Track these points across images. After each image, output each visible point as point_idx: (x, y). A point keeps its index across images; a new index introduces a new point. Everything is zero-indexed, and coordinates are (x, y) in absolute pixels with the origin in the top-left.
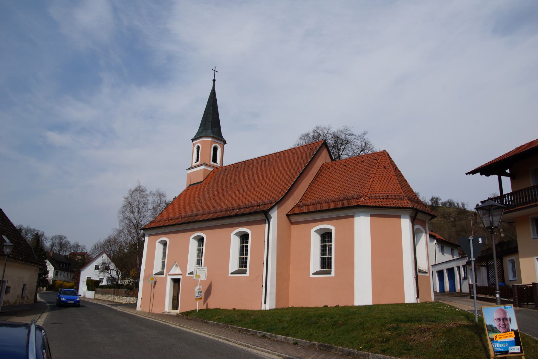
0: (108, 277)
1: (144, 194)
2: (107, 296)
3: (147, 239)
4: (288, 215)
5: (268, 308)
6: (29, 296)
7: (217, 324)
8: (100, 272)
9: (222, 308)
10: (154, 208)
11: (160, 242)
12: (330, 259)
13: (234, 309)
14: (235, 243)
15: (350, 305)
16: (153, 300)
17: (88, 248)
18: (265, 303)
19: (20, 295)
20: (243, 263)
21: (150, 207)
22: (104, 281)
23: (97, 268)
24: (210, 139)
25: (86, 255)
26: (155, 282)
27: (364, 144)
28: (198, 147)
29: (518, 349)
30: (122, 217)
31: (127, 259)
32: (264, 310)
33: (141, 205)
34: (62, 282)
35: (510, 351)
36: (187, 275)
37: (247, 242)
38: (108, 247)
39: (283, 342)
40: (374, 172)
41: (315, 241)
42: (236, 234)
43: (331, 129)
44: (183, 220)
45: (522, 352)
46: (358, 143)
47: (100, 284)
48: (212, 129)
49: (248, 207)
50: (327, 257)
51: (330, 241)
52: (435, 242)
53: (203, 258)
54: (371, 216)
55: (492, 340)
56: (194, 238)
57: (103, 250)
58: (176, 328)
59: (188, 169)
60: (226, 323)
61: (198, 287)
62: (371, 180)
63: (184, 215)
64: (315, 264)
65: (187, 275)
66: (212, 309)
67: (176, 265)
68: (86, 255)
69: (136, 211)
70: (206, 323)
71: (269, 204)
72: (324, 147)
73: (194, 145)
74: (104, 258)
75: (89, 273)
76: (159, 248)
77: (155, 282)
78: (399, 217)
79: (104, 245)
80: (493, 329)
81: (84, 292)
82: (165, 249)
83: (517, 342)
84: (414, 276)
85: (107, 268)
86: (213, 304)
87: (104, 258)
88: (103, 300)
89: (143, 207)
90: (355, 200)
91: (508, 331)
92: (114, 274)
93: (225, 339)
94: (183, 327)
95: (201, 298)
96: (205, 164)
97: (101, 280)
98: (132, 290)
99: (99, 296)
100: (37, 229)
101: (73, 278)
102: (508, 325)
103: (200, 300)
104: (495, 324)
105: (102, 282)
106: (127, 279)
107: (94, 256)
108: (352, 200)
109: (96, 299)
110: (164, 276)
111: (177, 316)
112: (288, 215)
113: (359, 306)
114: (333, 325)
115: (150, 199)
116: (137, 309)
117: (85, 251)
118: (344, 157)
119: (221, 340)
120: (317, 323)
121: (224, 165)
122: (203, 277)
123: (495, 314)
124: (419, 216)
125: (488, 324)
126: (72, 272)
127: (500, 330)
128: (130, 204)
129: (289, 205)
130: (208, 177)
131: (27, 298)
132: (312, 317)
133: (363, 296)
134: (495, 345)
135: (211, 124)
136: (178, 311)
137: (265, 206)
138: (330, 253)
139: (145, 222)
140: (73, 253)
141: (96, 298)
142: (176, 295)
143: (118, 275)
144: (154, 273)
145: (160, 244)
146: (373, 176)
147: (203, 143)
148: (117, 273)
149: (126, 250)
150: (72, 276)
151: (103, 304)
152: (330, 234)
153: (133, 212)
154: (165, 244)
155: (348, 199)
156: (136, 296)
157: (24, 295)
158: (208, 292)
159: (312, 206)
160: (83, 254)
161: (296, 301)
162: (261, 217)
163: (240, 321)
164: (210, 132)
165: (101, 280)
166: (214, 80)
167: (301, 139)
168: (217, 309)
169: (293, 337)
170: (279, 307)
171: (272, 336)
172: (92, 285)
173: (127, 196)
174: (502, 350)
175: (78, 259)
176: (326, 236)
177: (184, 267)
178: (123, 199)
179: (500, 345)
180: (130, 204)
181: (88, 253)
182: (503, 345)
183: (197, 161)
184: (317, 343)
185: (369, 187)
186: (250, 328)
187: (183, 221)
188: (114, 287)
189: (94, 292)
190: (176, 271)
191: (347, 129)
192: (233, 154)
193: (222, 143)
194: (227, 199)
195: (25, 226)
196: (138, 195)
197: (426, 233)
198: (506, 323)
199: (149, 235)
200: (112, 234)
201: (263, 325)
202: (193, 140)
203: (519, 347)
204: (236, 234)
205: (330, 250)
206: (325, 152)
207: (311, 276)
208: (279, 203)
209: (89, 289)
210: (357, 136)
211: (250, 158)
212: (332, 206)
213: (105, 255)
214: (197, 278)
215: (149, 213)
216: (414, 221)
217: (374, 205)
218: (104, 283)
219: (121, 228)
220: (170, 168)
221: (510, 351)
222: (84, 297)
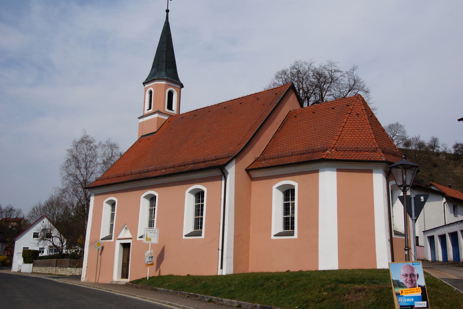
0: (50, 247)
1: (92, 145)
2: (48, 268)
3: (92, 199)
4: (248, 170)
5: (224, 273)
7: (166, 291)
8: (40, 240)
9: (174, 275)
10: (104, 163)
11: (108, 202)
12: (293, 218)
13: (188, 275)
14: (190, 202)
15: (313, 269)
16: (101, 268)
17: (25, 210)
18: (222, 268)
20: (198, 224)
21: (100, 160)
22: (46, 251)
23: (36, 235)
24: (164, 83)
25: (22, 222)
26: (103, 248)
27: (352, 82)
28: (151, 92)
29: (424, 304)
30: (65, 174)
31: (71, 225)
32: (220, 276)
33: (89, 159)
36: (138, 239)
37: (203, 201)
38: (50, 210)
39: (228, 306)
40: (345, 120)
41: (278, 199)
42: (190, 192)
43: (313, 65)
44: (133, 177)
46: (345, 81)
47: (40, 255)
48: (166, 71)
49: (204, 162)
50: (290, 216)
51: (293, 199)
52: (444, 200)
53: (155, 219)
54: (338, 170)
55: (398, 294)
56: (145, 197)
57: (44, 214)
58: (121, 296)
60: (176, 289)
61: (149, 252)
62: (341, 129)
63: (134, 171)
64: (277, 225)
65: (138, 239)
66: (165, 276)
67: (126, 228)
68: (23, 221)
69: (83, 165)
70: (155, 290)
71: (226, 158)
72: (291, 91)
73: (146, 89)
74: (45, 223)
75: (26, 241)
76: (107, 209)
77: (103, 248)
78: (371, 171)
79: (45, 208)
80: (399, 284)
81: (20, 266)
82: (113, 210)
83: (424, 298)
84: (388, 238)
85: (49, 236)
86: (166, 270)
87: (45, 223)
88: (42, 274)
89: (91, 161)
90: (320, 153)
91: (415, 287)
92: (57, 241)
93: (169, 304)
94: (128, 295)
95: (152, 264)
97: (42, 250)
98: (76, 260)
99: (38, 270)
101: (6, 250)
102: (415, 281)
103: (152, 266)
104: (402, 280)
105: (43, 252)
106: (73, 248)
107: (32, 222)
108: (317, 153)
109: (35, 273)
110: (113, 240)
111: (127, 285)
112: (248, 170)
113: (324, 271)
114: (277, 287)
115: (100, 152)
117: (21, 216)
118: (328, 98)
119: (164, 305)
120: (263, 285)
121: (181, 113)
122: (155, 240)
125: (394, 279)
126: (5, 242)
127: (407, 286)
128: (75, 158)
129: (249, 159)
130: (163, 127)
132: (259, 279)
133: (328, 259)
134: (400, 300)
135: (165, 65)
136: (128, 280)
137: (222, 160)
138: (293, 212)
139: (92, 179)
140: (6, 219)
141: (34, 271)
142: (126, 262)
143: (62, 243)
144: (101, 238)
145: (107, 204)
146: (343, 125)
147: (156, 87)
148: (61, 240)
149: (73, 214)
150: (4, 248)
151: (43, 277)
152: (293, 191)
153: (78, 168)
154: (113, 204)
155: (313, 152)
156: (81, 266)
158: (161, 258)
159: (274, 160)
160: (19, 220)
161: (257, 265)
162: (217, 173)
163: (189, 287)
165: (42, 250)
166: (167, 11)
167: (277, 77)
168: (170, 276)
169: (238, 300)
170: (237, 273)
171: (218, 300)
172: (30, 256)
174: (408, 304)
175: (12, 227)
176: (289, 193)
177: (134, 230)
178: (66, 152)
180: (75, 158)
181: (26, 218)
183: (150, 108)
184: (258, 305)
185: (337, 138)
186: (199, 293)
187: (133, 178)
188: (58, 257)
189: (32, 265)
190: (125, 234)
191: (331, 64)
192: (194, 97)
193: (179, 87)
194: (184, 152)
196: (85, 146)
198: (413, 279)
199: (95, 195)
200: (53, 194)
201: (212, 289)
202: (144, 84)
203: (425, 302)
204: (190, 192)
205: (293, 208)
206: (292, 98)
207: (273, 237)
208: (237, 157)
209: (26, 261)
210: (344, 72)
211: (210, 105)
212: (294, 160)
213: (45, 220)
214: (148, 242)
215: (99, 168)
216: (389, 176)
217: (341, 158)
218: (45, 253)
219: (64, 187)
220: (121, 116)
222: (20, 271)
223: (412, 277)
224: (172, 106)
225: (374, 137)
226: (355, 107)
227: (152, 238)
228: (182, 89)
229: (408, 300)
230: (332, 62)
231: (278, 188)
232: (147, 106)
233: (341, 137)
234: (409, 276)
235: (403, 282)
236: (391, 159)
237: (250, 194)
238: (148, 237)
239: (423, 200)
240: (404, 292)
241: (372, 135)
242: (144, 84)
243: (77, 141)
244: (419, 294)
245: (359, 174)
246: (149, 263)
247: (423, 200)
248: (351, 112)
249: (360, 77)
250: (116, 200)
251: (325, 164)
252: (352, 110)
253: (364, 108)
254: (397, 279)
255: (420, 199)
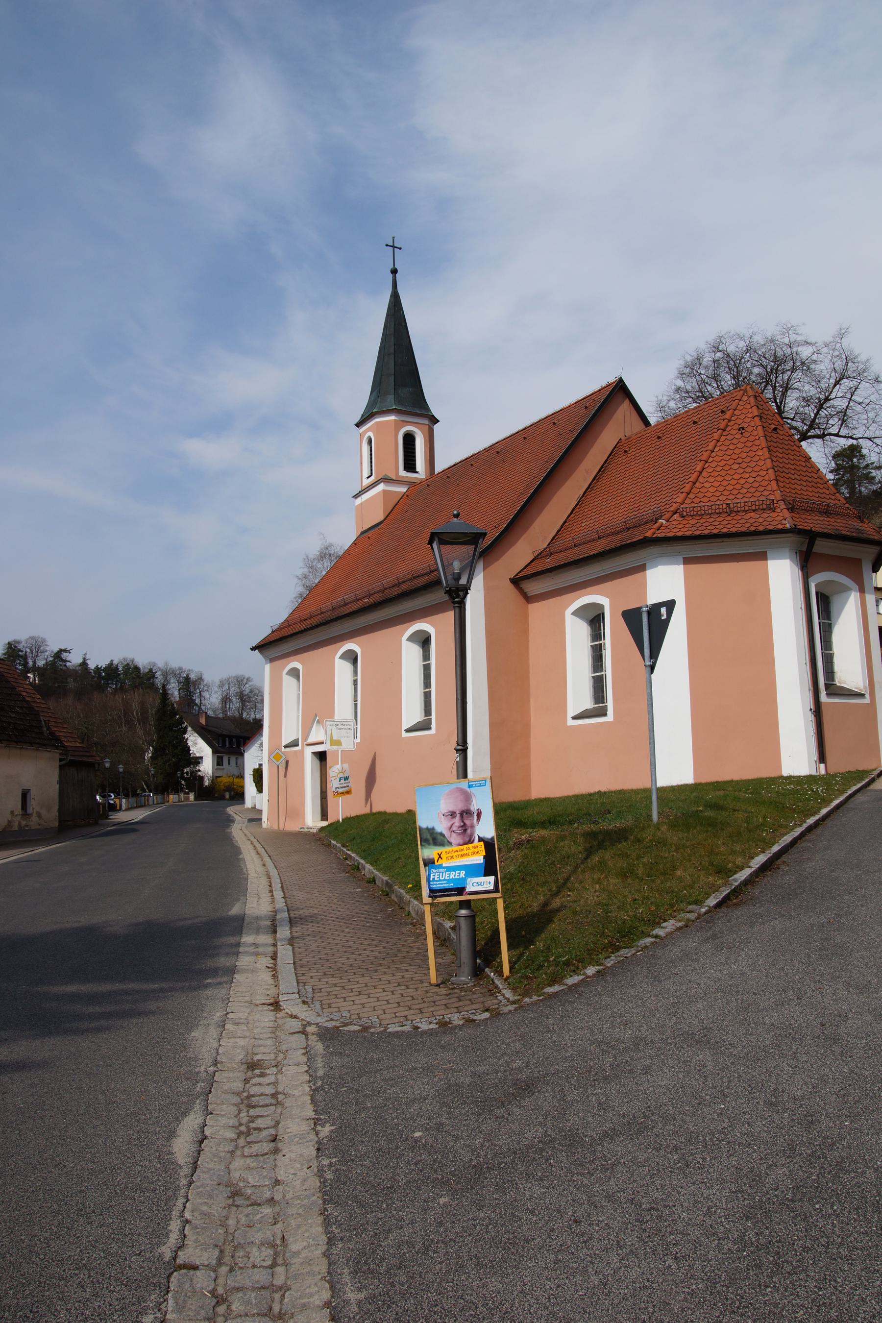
4: (516, 581)
6: (44, 812)
19: (18, 810)
24: (392, 418)
29: (488, 883)
34: (231, 779)
35: (469, 889)
45: (496, 890)
54: (687, 561)
55: (429, 863)
59: (356, 496)
73: (361, 436)
77: (287, 762)
78: (762, 556)
80: (434, 838)
81: (253, 797)
83: (489, 868)
84: (810, 703)
91: (471, 841)
96: (386, 480)
100: (186, 666)
102: (472, 826)
103: (348, 796)
104: (441, 826)
112: (516, 581)
116: (264, 825)
123: (442, 802)
124: (821, 546)
125: (424, 826)
127: (452, 840)
129: (519, 555)
130: (397, 511)
131: (39, 815)
134: (435, 875)
135: (399, 381)
157: (30, 811)
164: (390, 401)
166: (394, 271)
173: (299, 572)
174: (451, 885)
178: (296, 580)
179: (446, 876)
182: (453, 875)
195: (160, 664)
197: (862, 590)
198: (468, 822)
202: (359, 425)
203: (492, 879)
207: (571, 722)
216: (808, 562)
221: (469, 889)
223: (465, 816)
224: (415, 464)
225: (773, 477)
226: (736, 412)
227: (342, 740)
228: (436, 427)
229: (452, 876)
230: (789, 326)
231: (577, 613)
232: (366, 473)
233: (698, 485)
234: (458, 816)
235: (446, 832)
236: (816, 523)
237: (525, 632)
238: (335, 738)
239: (664, 617)
240: (444, 856)
241: (771, 471)
242: (359, 425)
243: (311, 556)
244: (479, 859)
245: (735, 564)
246: (340, 790)
247: (664, 617)
248: (727, 426)
249: (856, 351)
250: (299, 666)
251: (654, 550)
252: (729, 421)
253: (756, 413)
254: (430, 826)
255: (660, 615)
